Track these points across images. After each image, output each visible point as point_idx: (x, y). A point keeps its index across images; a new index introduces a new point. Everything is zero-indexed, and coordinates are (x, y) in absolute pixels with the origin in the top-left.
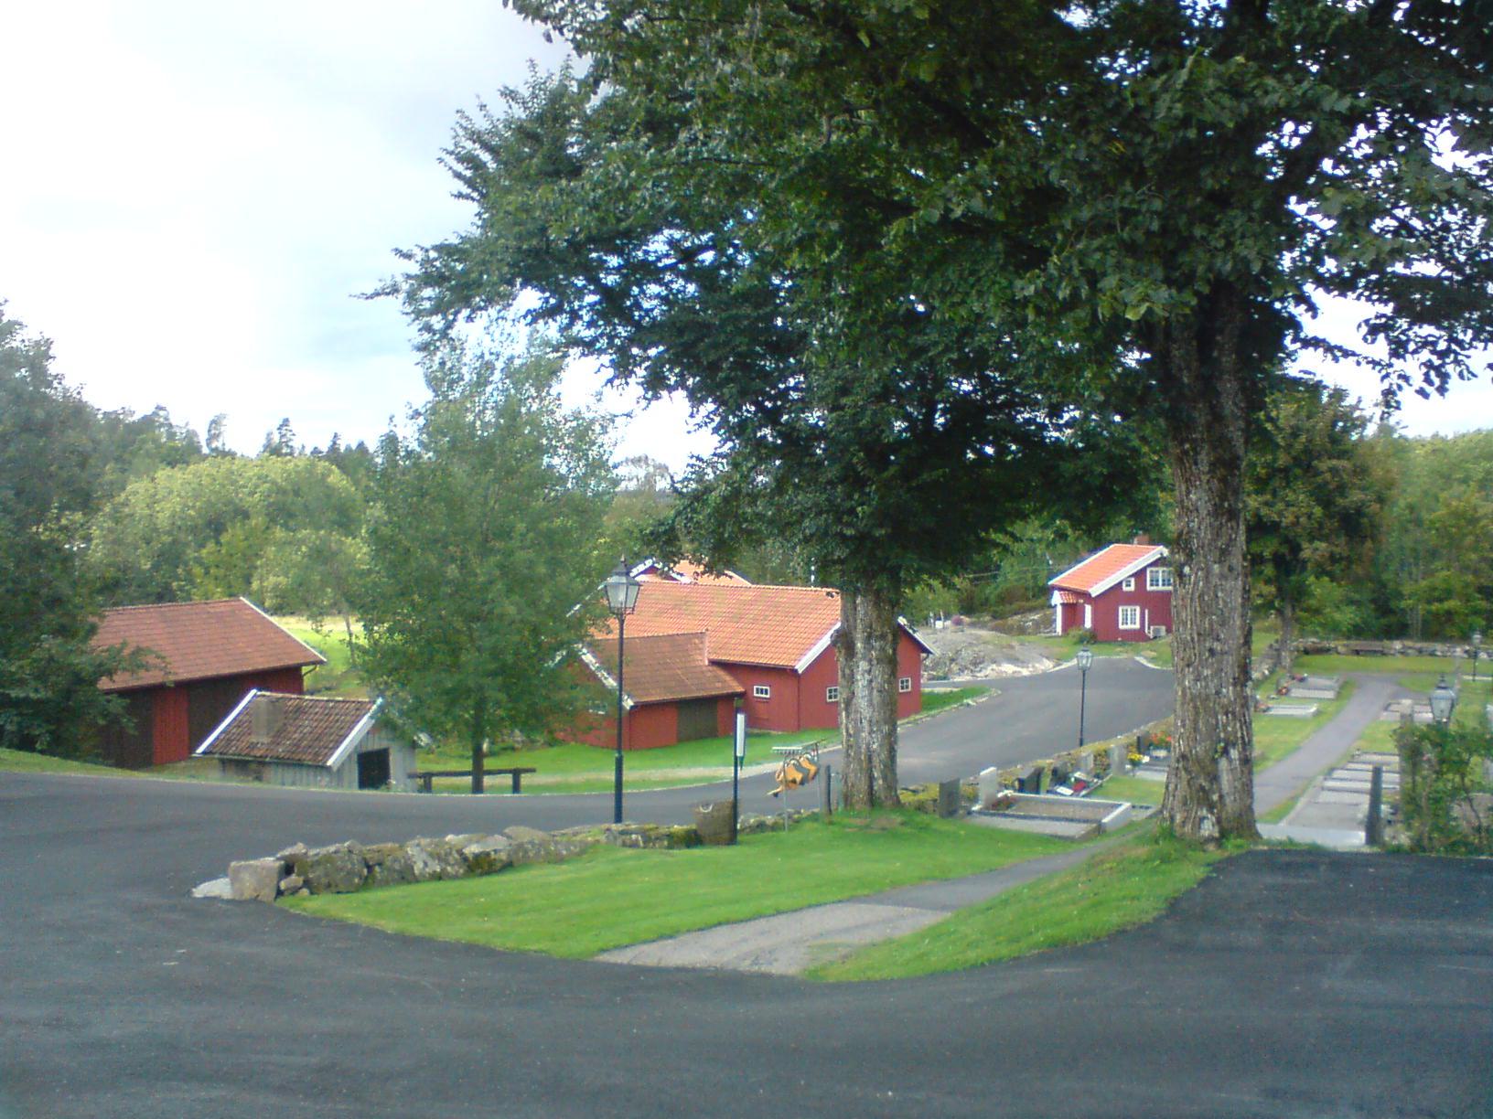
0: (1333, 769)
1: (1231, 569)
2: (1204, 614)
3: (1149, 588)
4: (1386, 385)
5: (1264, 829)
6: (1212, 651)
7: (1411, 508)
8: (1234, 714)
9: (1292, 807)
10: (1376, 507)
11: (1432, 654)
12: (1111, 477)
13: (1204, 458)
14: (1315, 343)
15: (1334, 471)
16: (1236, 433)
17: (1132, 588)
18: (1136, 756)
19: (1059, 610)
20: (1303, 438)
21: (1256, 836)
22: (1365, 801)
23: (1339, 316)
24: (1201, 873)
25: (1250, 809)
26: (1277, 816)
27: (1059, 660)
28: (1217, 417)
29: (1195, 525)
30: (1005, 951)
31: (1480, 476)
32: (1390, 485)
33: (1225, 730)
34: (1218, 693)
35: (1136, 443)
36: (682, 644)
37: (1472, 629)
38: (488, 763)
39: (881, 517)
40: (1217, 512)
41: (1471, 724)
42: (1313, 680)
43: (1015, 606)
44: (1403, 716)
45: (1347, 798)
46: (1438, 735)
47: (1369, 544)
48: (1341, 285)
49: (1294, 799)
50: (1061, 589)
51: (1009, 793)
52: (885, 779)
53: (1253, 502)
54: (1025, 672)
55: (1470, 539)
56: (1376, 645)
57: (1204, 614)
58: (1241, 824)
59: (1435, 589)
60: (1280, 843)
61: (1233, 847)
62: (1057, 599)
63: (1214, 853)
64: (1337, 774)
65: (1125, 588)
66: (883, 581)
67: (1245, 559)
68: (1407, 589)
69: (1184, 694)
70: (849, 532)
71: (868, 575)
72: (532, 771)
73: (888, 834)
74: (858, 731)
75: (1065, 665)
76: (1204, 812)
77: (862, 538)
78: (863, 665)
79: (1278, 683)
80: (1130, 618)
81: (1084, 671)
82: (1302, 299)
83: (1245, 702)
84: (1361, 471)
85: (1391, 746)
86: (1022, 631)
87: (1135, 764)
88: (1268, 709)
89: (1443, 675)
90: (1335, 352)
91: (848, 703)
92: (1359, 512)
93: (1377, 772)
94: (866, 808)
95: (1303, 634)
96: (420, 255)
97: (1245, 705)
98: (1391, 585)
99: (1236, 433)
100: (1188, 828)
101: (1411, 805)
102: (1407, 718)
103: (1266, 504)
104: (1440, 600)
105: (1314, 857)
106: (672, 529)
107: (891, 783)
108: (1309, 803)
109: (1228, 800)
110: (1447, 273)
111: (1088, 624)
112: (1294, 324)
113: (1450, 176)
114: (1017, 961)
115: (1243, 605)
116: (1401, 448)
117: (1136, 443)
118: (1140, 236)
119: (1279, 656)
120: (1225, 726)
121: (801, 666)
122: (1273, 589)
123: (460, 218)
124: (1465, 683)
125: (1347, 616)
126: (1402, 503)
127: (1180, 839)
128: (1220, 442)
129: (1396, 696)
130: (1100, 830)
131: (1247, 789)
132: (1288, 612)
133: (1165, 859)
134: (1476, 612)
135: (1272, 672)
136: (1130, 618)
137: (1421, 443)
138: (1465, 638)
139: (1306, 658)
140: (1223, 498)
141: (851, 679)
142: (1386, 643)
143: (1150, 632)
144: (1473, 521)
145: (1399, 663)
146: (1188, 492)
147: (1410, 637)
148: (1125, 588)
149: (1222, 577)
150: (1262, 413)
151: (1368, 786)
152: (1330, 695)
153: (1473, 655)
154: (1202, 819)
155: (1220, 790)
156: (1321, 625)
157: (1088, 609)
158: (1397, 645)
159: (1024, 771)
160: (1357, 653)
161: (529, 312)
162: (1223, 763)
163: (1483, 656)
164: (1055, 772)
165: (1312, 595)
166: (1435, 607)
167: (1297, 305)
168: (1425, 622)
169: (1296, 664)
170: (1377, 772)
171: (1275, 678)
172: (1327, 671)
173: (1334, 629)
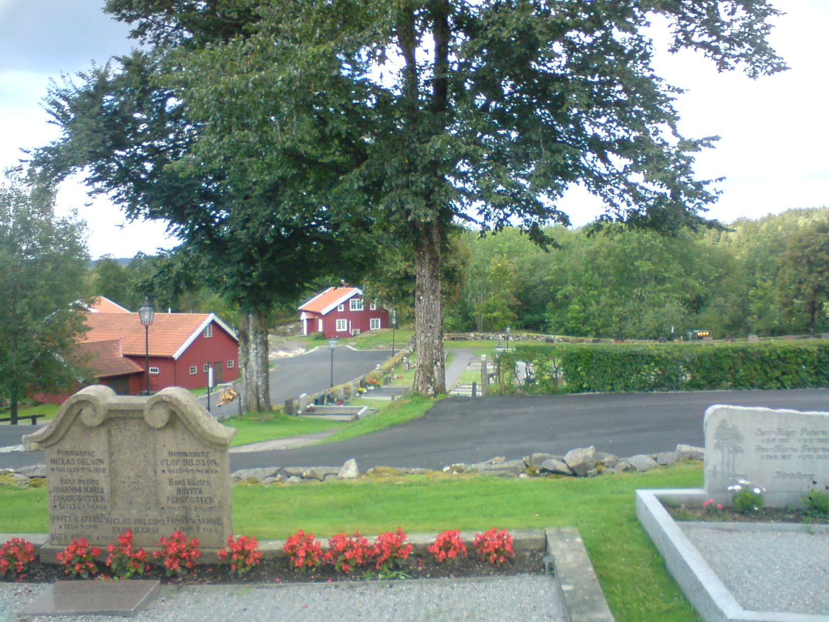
3: (351, 310)
7: (477, 267)
10: (461, 267)
11: (488, 338)
12: (365, 259)
13: (427, 257)
16: (437, 248)
17: (342, 310)
18: (361, 389)
19: (305, 323)
27: (308, 348)
28: (431, 243)
30: (370, 430)
31: (507, 250)
32: (468, 257)
35: (375, 243)
36: (108, 346)
38: (20, 413)
39: (262, 277)
40: (431, 277)
43: (280, 321)
47: (458, 285)
50: (306, 311)
51: (312, 405)
52: (265, 398)
54: (291, 355)
56: (462, 335)
59: (488, 306)
61: (440, 396)
62: (304, 316)
65: (339, 310)
66: (262, 307)
68: (476, 307)
70: (248, 284)
71: (255, 303)
72: (43, 416)
73: (268, 422)
74: (251, 377)
75: (311, 351)
77: (254, 287)
78: (253, 346)
80: (342, 325)
81: (332, 350)
82: (460, 200)
86: (285, 334)
87: (361, 393)
91: (246, 365)
92: (454, 270)
94: (256, 412)
96: (34, 152)
97: (442, 346)
98: (468, 305)
99: (437, 248)
103: (410, 266)
104: (491, 312)
106: (152, 283)
107: (267, 401)
111: (321, 329)
114: (380, 430)
117: (375, 243)
118: (419, 190)
121: (176, 356)
123: (56, 134)
126: (472, 265)
127: (421, 396)
128: (433, 251)
130: (357, 418)
131: (443, 377)
133: (418, 403)
134: (507, 318)
136: (342, 325)
138: (503, 330)
140: (434, 272)
141: (247, 353)
143: (352, 332)
145: (474, 343)
148: (339, 310)
157: (320, 322)
158: (472, 335)
159: (317, 395)
160: (453, 339)
161: (87, 179)
162: (435, 368)
163: (511, 338)
164: (328, 397)
166: (489, 315)
168: (484, 323)
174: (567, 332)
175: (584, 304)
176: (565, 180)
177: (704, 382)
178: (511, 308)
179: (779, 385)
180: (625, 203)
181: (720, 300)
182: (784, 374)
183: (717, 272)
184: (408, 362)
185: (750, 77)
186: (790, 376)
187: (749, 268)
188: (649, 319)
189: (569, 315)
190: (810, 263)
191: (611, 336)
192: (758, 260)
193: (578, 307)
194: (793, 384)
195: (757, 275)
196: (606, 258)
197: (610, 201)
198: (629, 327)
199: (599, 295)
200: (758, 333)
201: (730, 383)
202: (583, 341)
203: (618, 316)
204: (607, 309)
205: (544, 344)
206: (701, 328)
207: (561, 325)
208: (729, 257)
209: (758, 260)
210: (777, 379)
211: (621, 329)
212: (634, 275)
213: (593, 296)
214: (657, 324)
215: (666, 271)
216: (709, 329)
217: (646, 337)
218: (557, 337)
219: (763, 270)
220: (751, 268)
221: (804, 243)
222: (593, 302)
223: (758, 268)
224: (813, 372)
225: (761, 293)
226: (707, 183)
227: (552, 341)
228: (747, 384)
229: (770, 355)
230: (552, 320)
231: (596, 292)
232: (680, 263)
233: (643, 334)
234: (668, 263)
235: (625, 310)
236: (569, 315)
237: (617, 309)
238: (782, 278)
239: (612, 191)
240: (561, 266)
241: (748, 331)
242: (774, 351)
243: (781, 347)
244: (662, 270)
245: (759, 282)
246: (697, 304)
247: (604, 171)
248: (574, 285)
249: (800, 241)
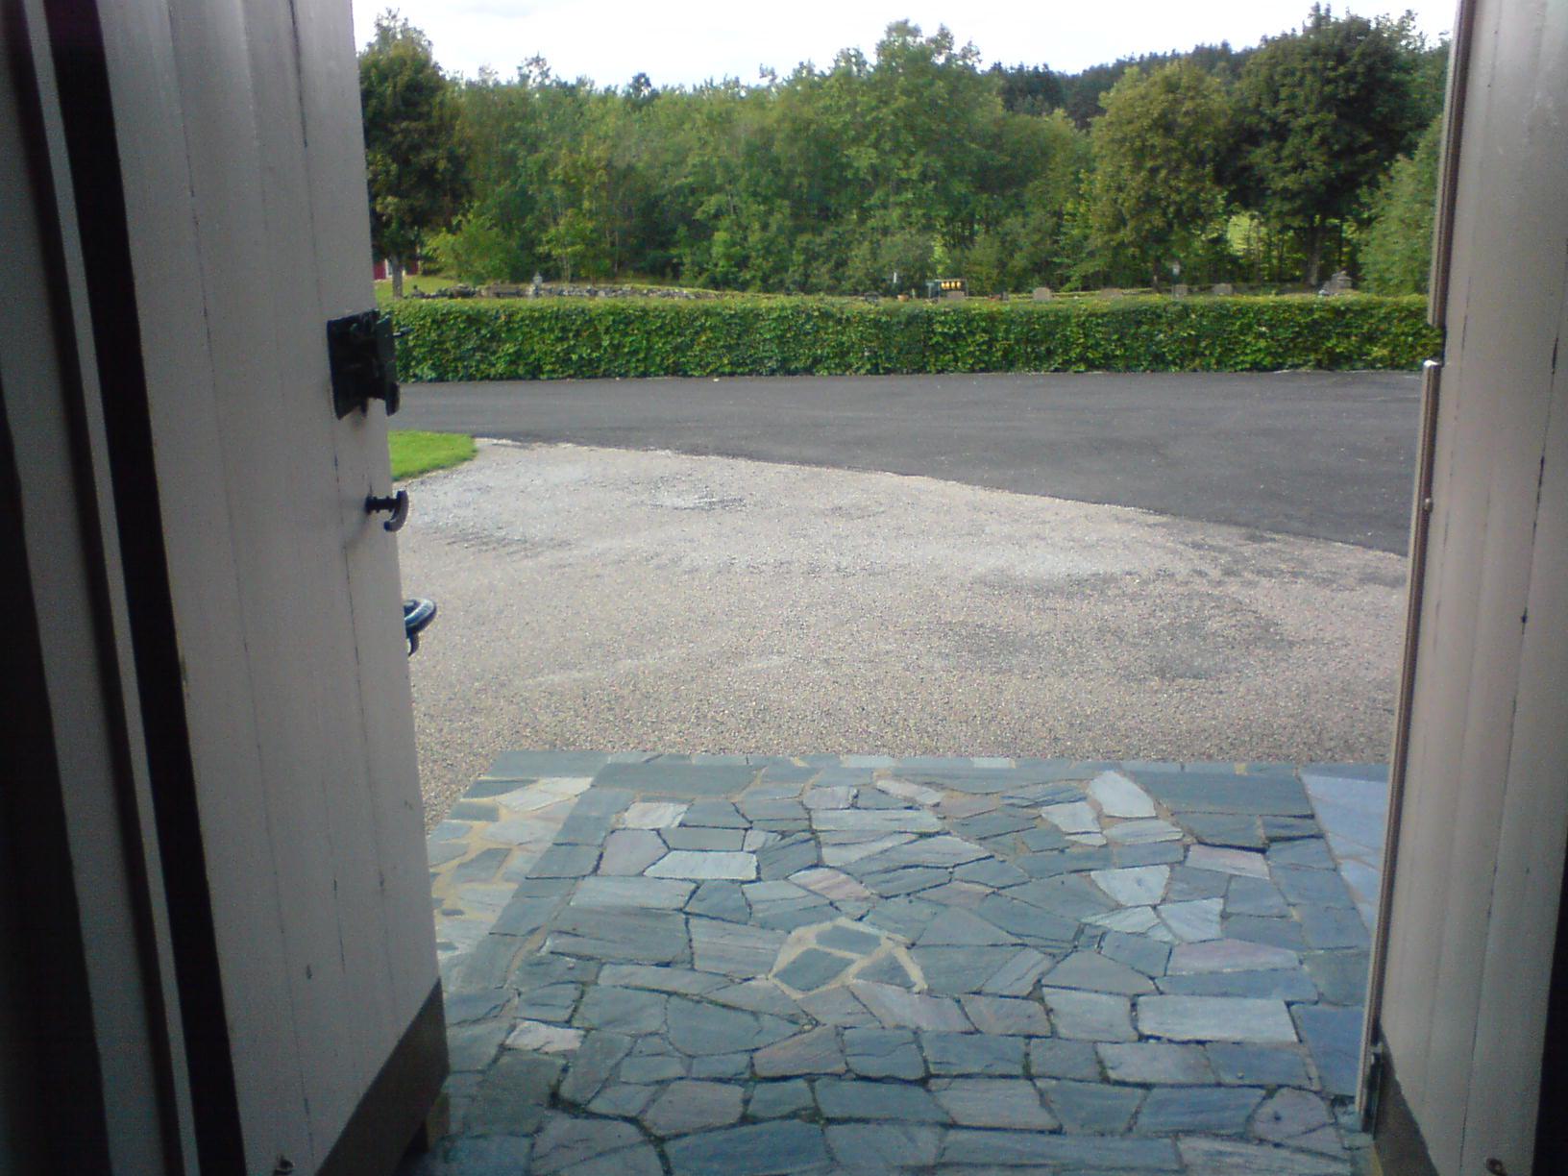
15: (406, 132)
137: (1248, 53)
196: (792, 139)
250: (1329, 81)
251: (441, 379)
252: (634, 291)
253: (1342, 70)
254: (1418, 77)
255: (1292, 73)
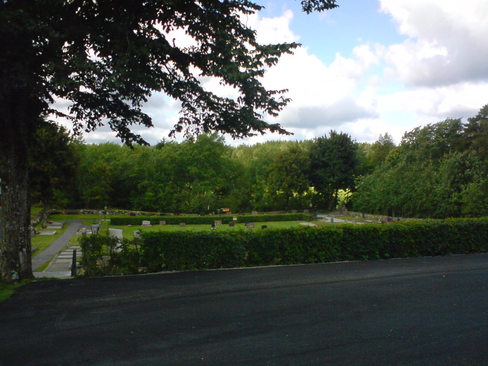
0: (61, 252)
1: (23, 187)
2: (13, 202)
4: (75, 127)
5: (36, 275)
6: (16, 215)
8: (24, 236)
9: (47, 265)
10: (74, 166)
11: (93, 213)
14: (53, 111)
15: (61, 154)
20: (50, 143)
21: (33, 277)
22: (71, 261)
23: (61, 104)
24: (11, 292)
25: (31, 269)
26: (43, 268)
29: (9, 171)
32: (79, 159)
33: (21, 242)
34: (18, 229)
37: (104, 205)
41: (104, 235)
42: (54, 223)
44: (83, 233)
45: (66, 261)
46: (93, 238)
48: (61, 94)
49: (48, 262)
53: (33, 164)
55: (103, 177)
56: (74, 211)
57: (13, 202)
58: (28, 273)
59: (93, 192)
60: (41, 279)
61: (24, 282)
63: (17, 285)
64: (62, 253)
67: (28, 183)
68: (84, 193)
69: (6, 230)
76: (13, 271)
79: (42, 224)
83: (29, 232)
84: (70, 155)
85: (78, 243)
88: (39, 233)
89: (95, 219)
90: (61, 115)
93: (75, 252)
95: (51, 207)
100: (7, 277)
101: (85, 262)
102: (84, 234)
104: (95, 196)
105: (54, 281)
108: (53, 264)
109: (22, 266)
110: (94, 93)
112: (46, 105)
113: (95, 63)
115: (27, 199)
116: (83, 147)
119: (43, 215)
120: (21, 240)
122: (40, 193)
124: (102, 221)
125: (65, 201)
129: (82, 227)
131: (29, 262)
132: (46, 201)
135: (40, 221)
137: (89, 146)
138: (102, 208)
139: (51, 216)
142: (78, 210)
144: (104, 171)
145: (82, 216)
146: (7, 160)
147: (85, 208)
149: (20, 189)
150: (34, 134)
151: (72, 256)
152: (60, 227)
153: (105, 213)
154: (13, 274)
155: (19, 262)
156: (57, 204)
158: (82, 211)
160: (69, 213)
163: (108, 213)
165: (53, 195)
166: (93, 198)
167: (46, 98)
169: (49, 218)
170: (75, 252)
171: (42, 222)
172: (59, 220)
173: (62, 206)
174: (144, 209)
175: (155, 192)
176: (148, 87)
177: (260, 259)
178: (107, 193)
179: (316, 260)
180: (201, 108)
181: (236, 191)
182: (319, 251)
183: (234, 174)
184: (34, 230)
185: (305, 10)
186: (324, 253)
187: (252, 173)
188: (194, 202)
189: (146, 198)
190: (286, 170)
191: (172, 212)
192: (257, 168)
193: (151, 194)
194: (326, 258)
195: (257, 176)
196: (170, 164)
197: (188, 105)
198: (183, 207)
199: (165, 186)
200: (257, 210)
201: (280, 259)
202: (154, 215)
203: (176, 199)
204: (169, 195)
205: (129, 217)
206: (224, 207)
207: (140, 205)
208: (240, 166)
209: (257, 168)
210: (316, 256)
211: (178, 207)
212: (187, 175)
213: (161, 187)
214: (199, 204)
215: (205, 173)
216: (229, 207)
217: (193, 212)
218: (138, 212)
219: (259, 174)
220: (253, 172)
221: (284, 159)
222: (161, 191)
223: (257, 173)
224: (340, 248)
225: (259, 187)
226: (273, 92)
227: (134, 215)
228: (292, 259)
229: (310, 236)
230: (135, 202)
231: (162, 185)
232: (214, 169)
233: (191, 210)
234: (207, 169)
235: (180, 196)
236: (146, 198)
237: (175, 195)
238: (271, 179)
239: (190, 97)
240: (141, 168)
241: (251, 209)
242: (313, 233)
243: (318, 230)
244: (203, 172)
245: (258, 181)
246: (224, 192)
247: (183, 78)
248: (148, 180)
249: (281, 157)
250: (340, 151)
251: (167, 224)
252: (119, 212)
253: (343, 148)
254: (358, 151)
255: (329, 148)
